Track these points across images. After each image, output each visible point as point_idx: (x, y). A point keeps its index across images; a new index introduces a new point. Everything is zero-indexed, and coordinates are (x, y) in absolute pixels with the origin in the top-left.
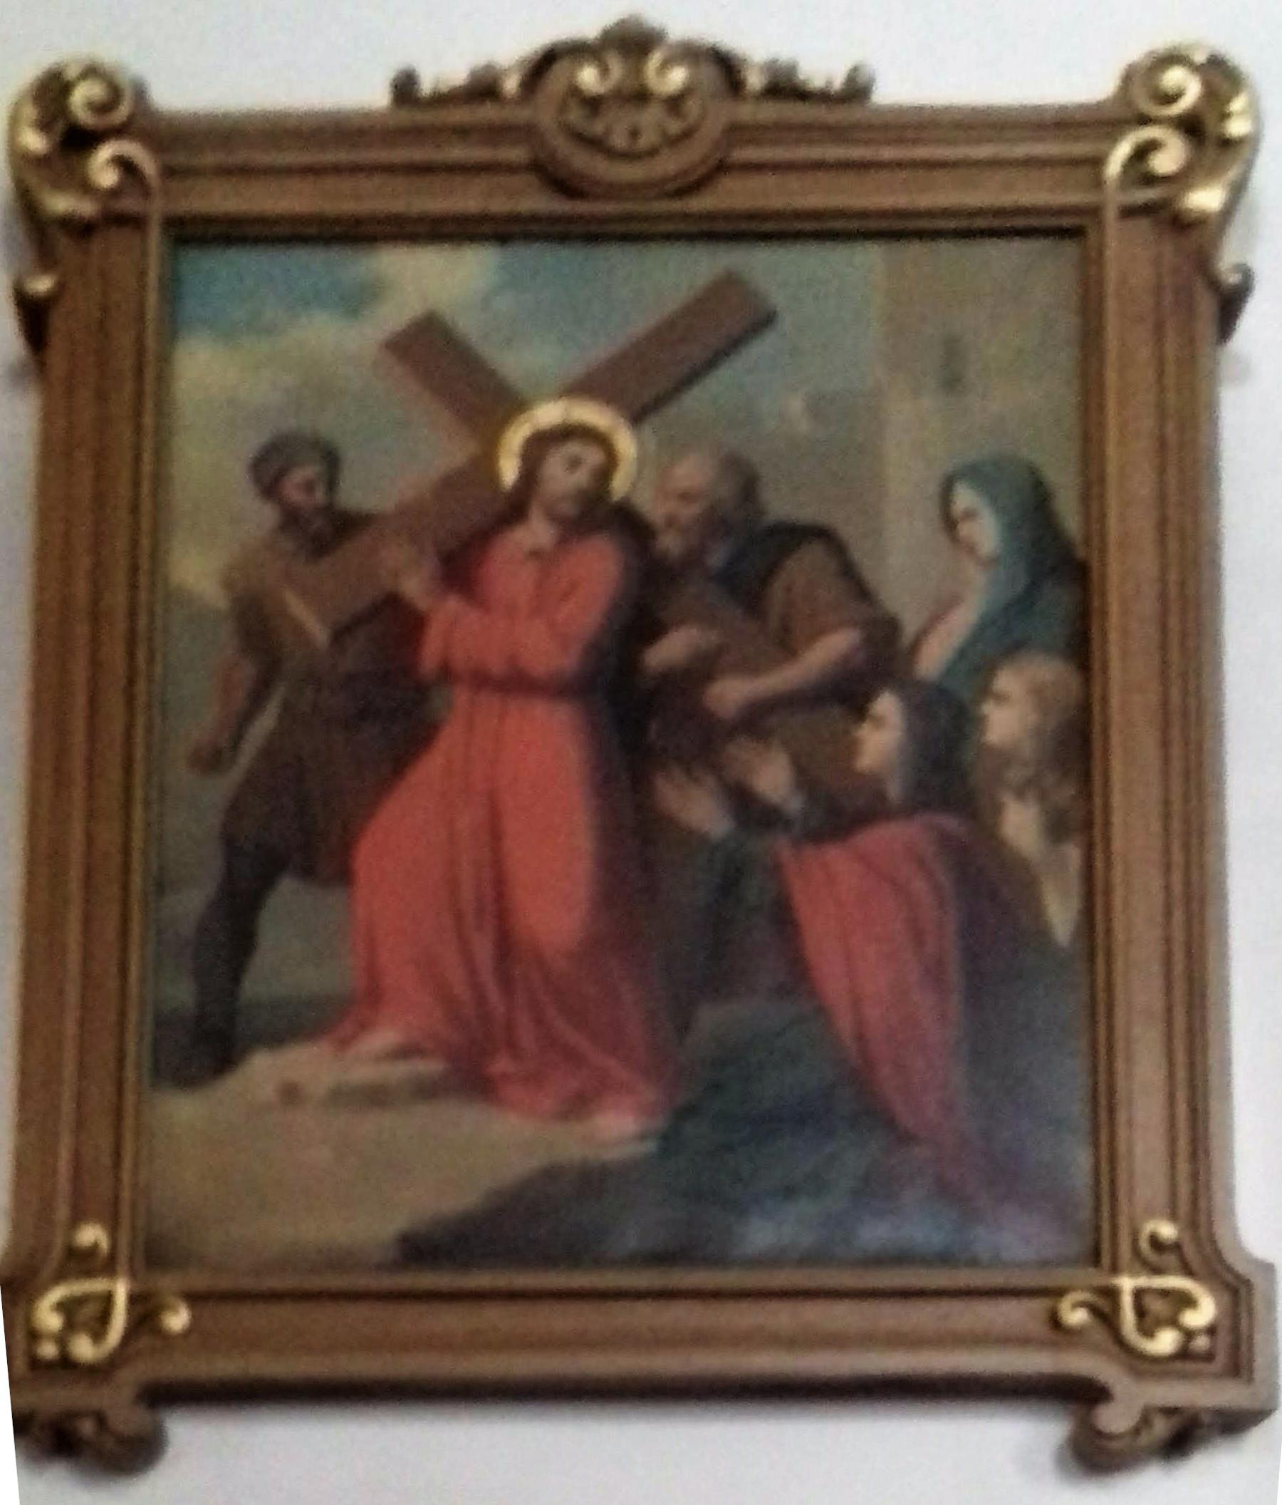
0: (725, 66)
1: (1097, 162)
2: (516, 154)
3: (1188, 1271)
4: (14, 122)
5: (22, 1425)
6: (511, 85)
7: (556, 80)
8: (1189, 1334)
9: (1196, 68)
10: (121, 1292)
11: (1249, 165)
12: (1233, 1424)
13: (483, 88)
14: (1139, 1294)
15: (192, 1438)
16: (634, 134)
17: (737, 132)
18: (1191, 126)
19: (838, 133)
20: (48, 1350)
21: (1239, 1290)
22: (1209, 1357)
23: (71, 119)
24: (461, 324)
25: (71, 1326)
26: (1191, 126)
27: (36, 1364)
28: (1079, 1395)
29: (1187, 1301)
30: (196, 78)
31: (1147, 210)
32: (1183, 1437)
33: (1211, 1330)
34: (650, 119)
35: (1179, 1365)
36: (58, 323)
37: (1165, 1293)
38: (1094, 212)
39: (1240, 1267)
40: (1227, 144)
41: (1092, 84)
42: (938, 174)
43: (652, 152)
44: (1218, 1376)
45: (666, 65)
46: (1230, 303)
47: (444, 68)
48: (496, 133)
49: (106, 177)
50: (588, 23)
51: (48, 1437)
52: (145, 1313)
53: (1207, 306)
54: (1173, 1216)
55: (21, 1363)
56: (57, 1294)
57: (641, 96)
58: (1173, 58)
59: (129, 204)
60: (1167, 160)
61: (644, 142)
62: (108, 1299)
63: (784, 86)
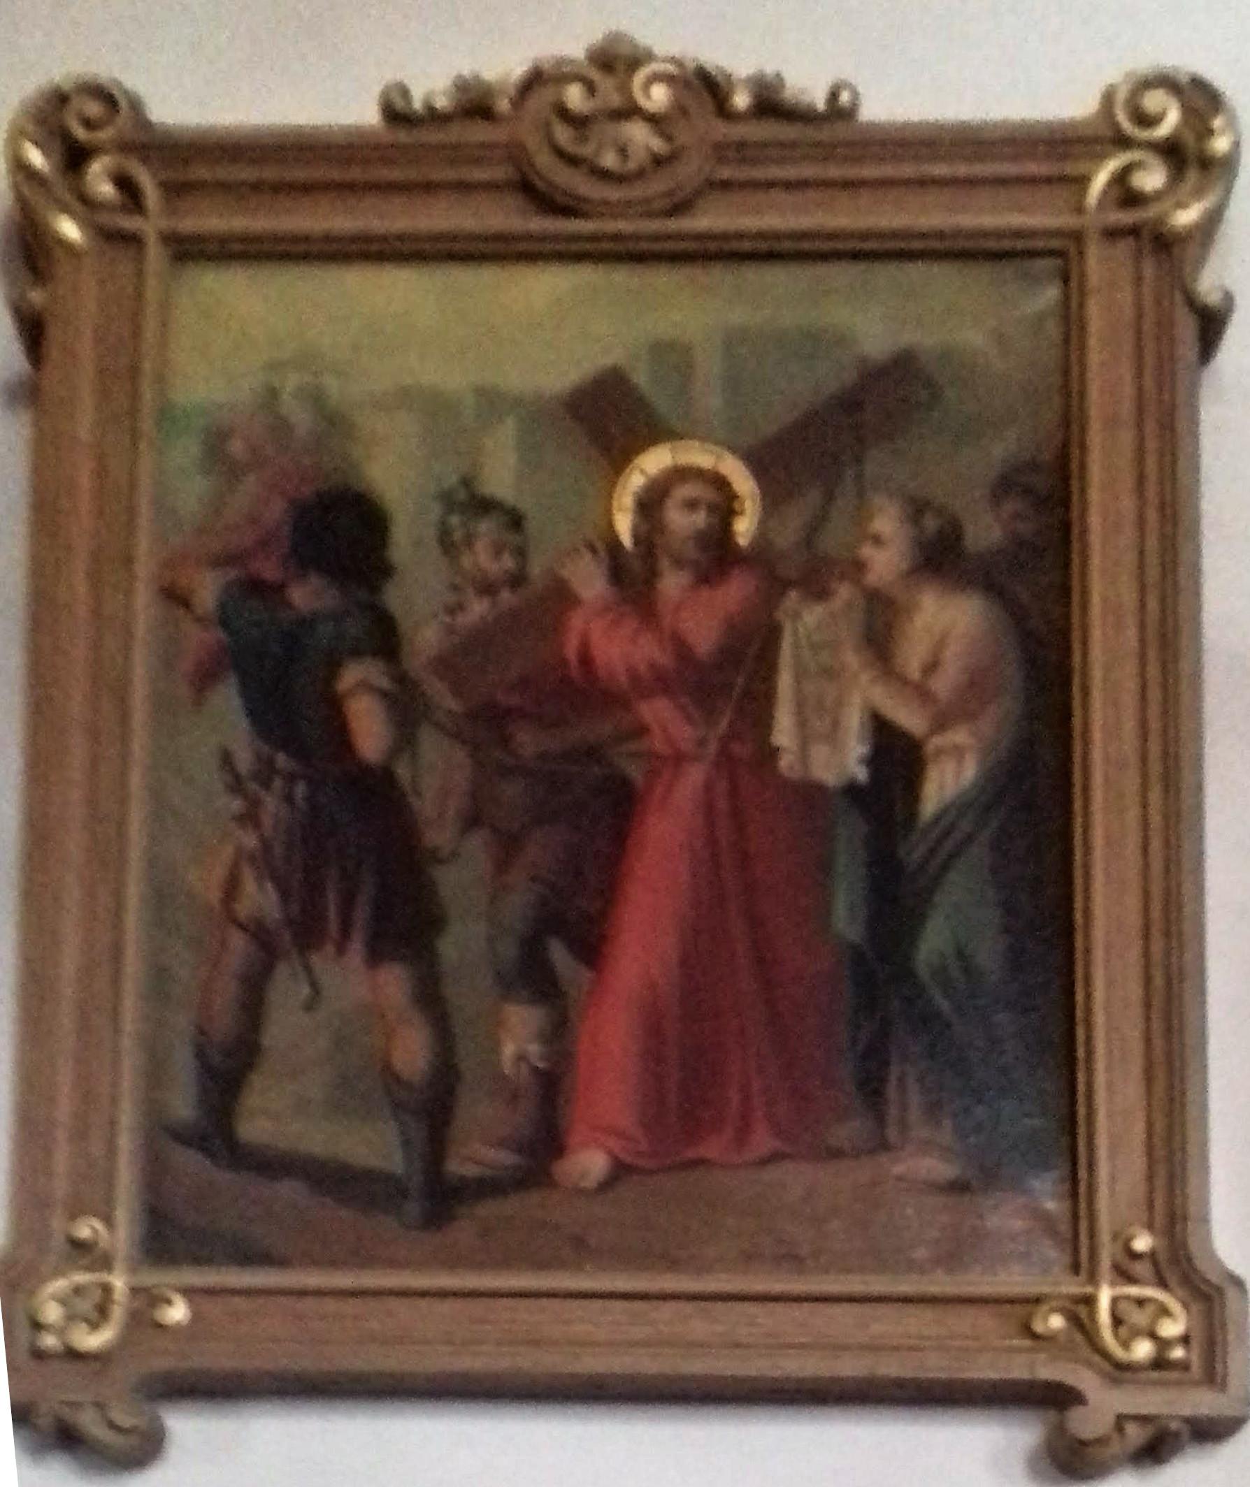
0: (706, 86)
1: (1082, 182)
2: (499, 173)
3: (1162, 1283)
4: (17, 135)
5: (22, 1416)
6: (503, 105)
7: (540, 100)
8: (1163, 1344)
10: (119, 1282)
11: (1228, 191)
12: (1210, 1432)
13: (475, 104)
14: (1115, 1301)
16: (623, 151)
17: (721, 151)
19: (827, 152)
21: (1207, 1292)
22: (1184, 1366)
24: (1132, 723)
25: (71, 1318)
27: (39, 1355)
28: (1055, 1399)
29: (1165, 1312)
30: (182, 99)
31: (1134, 231)
32: (1156, 1448)
33: (1185, 1340)
34: (639, 135)
35: (1155, 1375)
36: (54, 333)
37: (1141, 1302)
38: (1077, 236)
39: (1214, 1278)
41: (1068, 99)
43: (640, 174)
44: (1196, 1384)
45: (656, 78)
46: (1211, 325)
47: (430, 84)
50: (574, 46)
51: (47, 1429)
52: (147, 1300)
53: (1187, 328)
54: (1150, 1227)
55: (23, 1357)
56: (59, 1285)
57: (630, 111)
58: (1166, 82)
59: (129, 223)
63: (770, 103)
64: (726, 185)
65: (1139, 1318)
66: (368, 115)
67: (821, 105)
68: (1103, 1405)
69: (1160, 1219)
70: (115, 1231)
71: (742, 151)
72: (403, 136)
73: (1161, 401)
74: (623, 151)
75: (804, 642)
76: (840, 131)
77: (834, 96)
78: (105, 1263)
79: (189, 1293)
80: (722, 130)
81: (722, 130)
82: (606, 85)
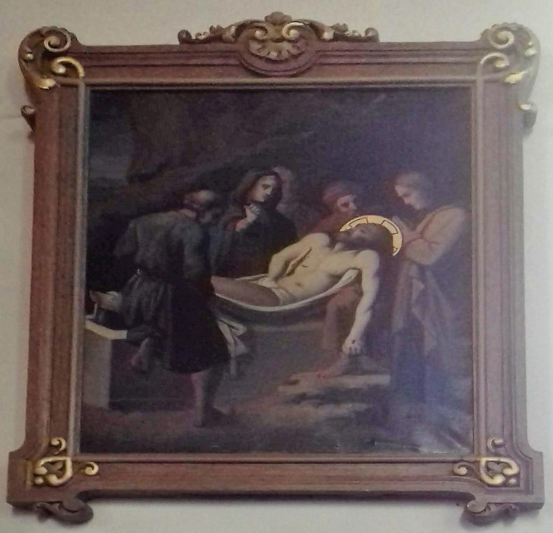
0: (314, 29)
1: (475, 63)
9: (514, 32)
13: (216, 36)
15: (102, 511)
16: (280, 52)
18: (509, 51)
20: (40, 481)
21: (528, 461)
23: (41, 51)
26: (509, 51)
29: (509, 466)
32: (507, 514)
33: (517, 476)
37: (498, 463)
40: (529, 59)
41: (472, 35)
42: (393, 67)
43: (286, 60)
47: (199, 28)
48: (225, 54)
49: (62, 70)
52: (79, 467)
54: (503, 437)
56: (42, 462)
58: (505, 28)
60: (501, 65)
61: (285, 55)
62: (64, 463)
63: (340, 35)
64: (322, 64)
65: (496, 468)
66: (177, 42)
67: (363, 35)
68: (481, 500)
69: (506, 433)
70: (69, 443)
71: (323, 54)
72: (185, 47)
73: (217, 217)
74: (280, 52)
75: (212, 262)
76: (373, 47)
77: (367, 31)
78: (64, 452)
79: (98, 463)
80: (318, 46)
81: (318, 46)
82: (271, 30)
